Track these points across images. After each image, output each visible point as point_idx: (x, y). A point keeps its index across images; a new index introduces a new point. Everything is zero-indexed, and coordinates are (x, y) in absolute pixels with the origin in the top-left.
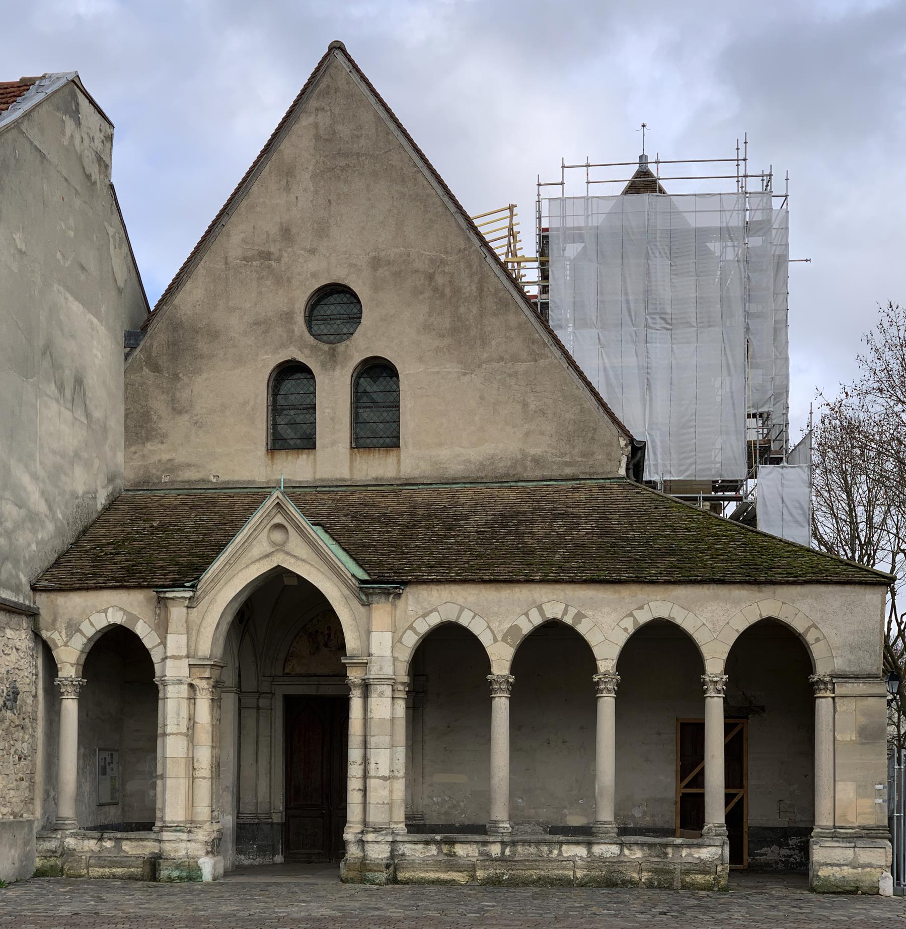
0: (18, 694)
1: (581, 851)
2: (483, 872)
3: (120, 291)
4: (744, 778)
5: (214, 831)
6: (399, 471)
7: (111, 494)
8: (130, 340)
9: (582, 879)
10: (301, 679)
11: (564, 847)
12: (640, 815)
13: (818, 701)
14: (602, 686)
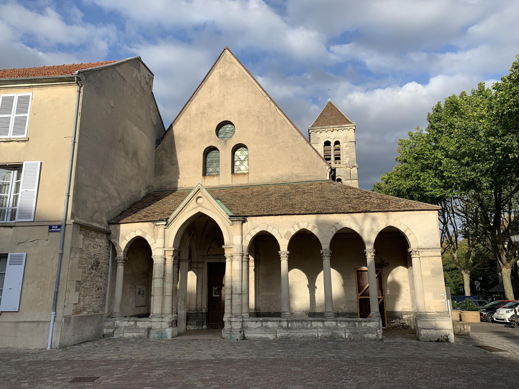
0: (99, 264)
1: (320, 324)
2: (280, 334)
3: (155, 126)
5: (173, 317)
7: (148, 192)
9: (321, 337)
10: (214, 256)
11: (313, 323)
12: (344, 308)
13: (413, 259)
14: (324, 255)
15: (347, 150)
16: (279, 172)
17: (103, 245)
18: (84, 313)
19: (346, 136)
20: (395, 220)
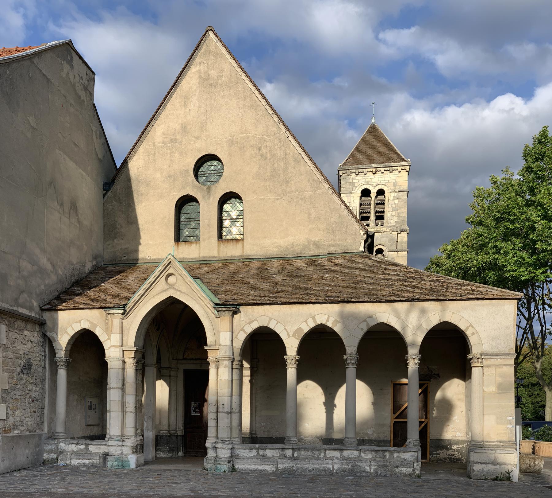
1: (337, 454)
2: (282, 465)
4: (428, 413)
5: (137, 441)
6: (243, 252)
7: (95, 265)
8: (106, 187)
9: (337, 470)
11: (327, 452)
12: (371, 433)
13: (473, 369)
14: (349, 361)
15: (395, 204)
16: (290, 240)
17: (36, 340)
18: (15, 432)
19: (395, 181)
20: (453, 313)
